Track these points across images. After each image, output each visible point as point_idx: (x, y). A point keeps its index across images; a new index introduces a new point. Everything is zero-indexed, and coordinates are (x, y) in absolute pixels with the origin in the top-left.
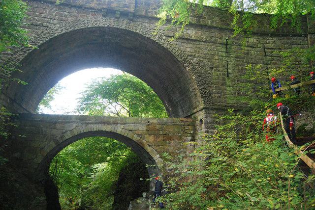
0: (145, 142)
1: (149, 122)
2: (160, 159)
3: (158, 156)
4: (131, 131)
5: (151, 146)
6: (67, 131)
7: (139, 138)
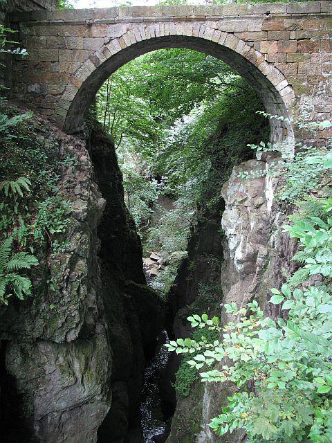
0: (258, 55)
2: (289, 89)
3: (285, 83)
4: (233, 33)
5: (273, 63)
6: (111, 40)
7: (247, 48)
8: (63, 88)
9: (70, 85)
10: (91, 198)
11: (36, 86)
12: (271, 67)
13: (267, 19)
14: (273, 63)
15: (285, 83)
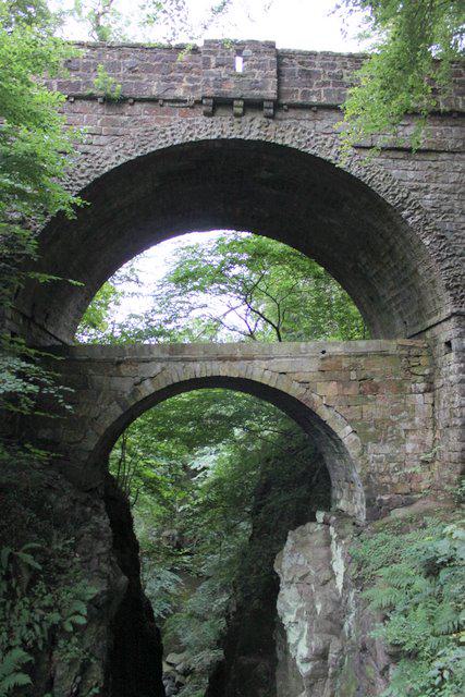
1: (324, 352)
2: (354, 437)
3: (349, 429)
5: (333, 407)
6: (143, 380)
8: (82, 436)
9: (90, 431)
10: (112, 576)
11: (49, 431)
12: (332, 411)
13: (323, 359)
14: (333, 407)
15: (349, 429)
